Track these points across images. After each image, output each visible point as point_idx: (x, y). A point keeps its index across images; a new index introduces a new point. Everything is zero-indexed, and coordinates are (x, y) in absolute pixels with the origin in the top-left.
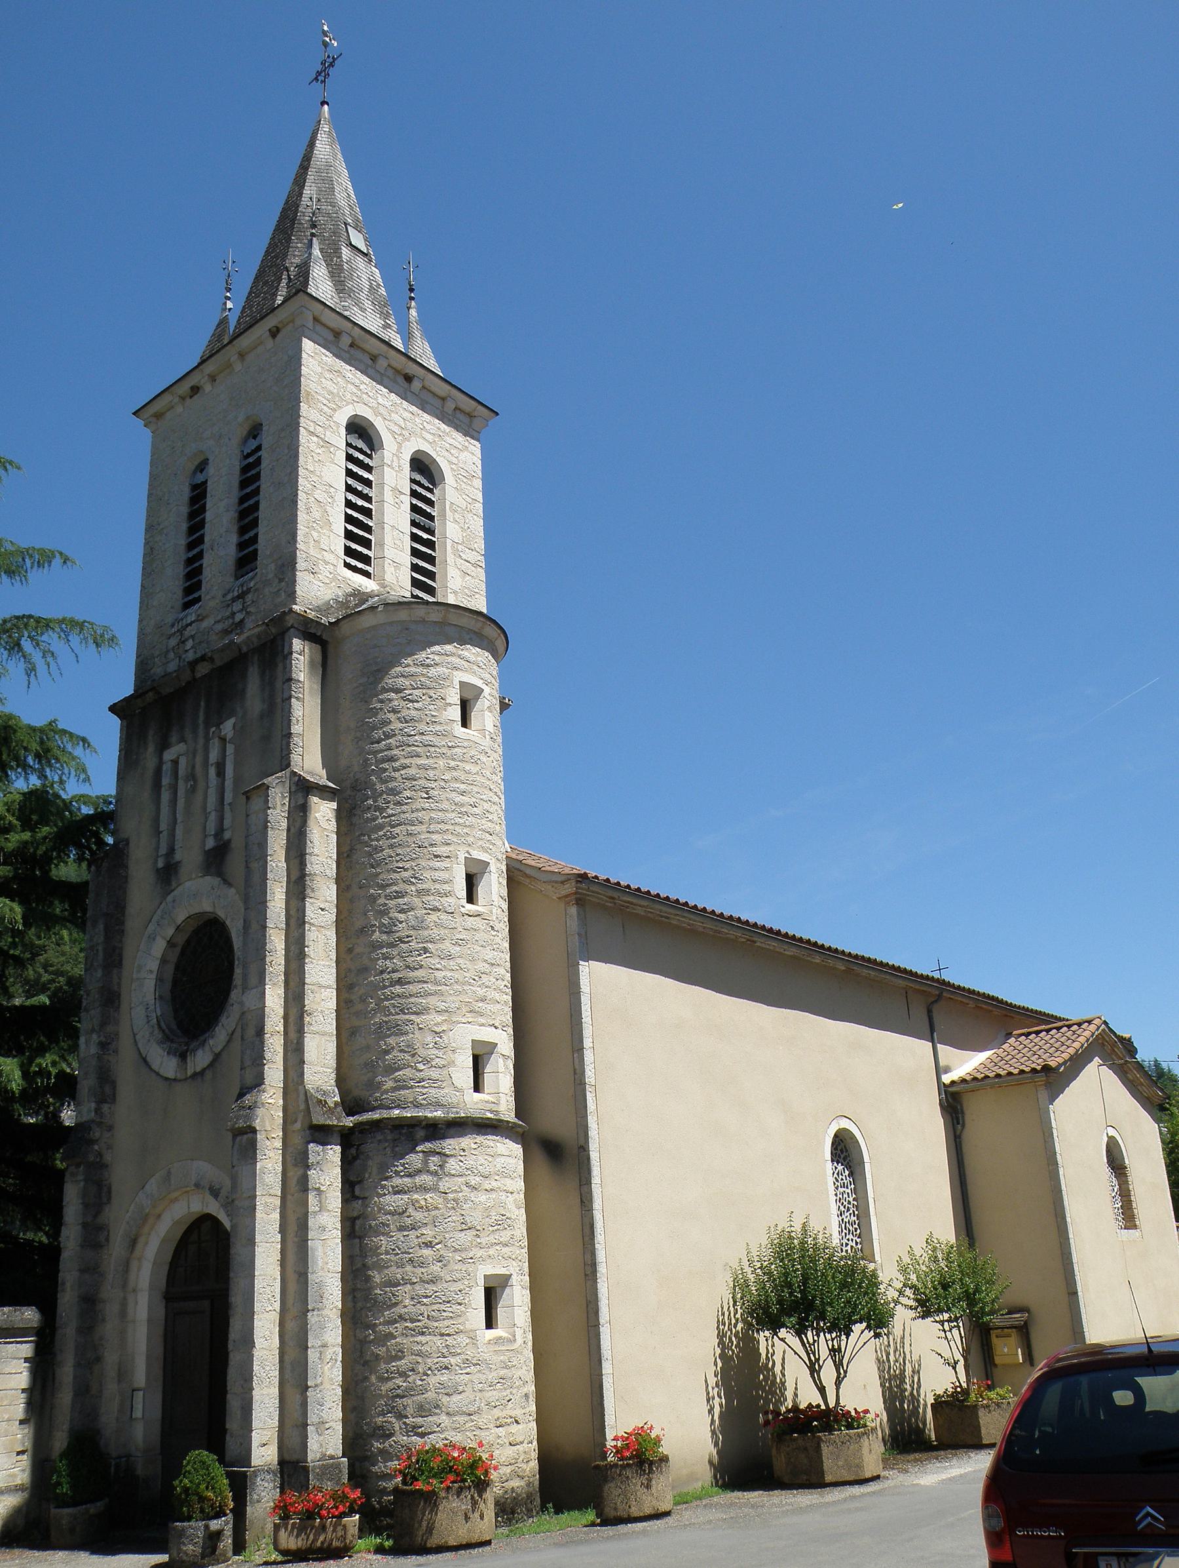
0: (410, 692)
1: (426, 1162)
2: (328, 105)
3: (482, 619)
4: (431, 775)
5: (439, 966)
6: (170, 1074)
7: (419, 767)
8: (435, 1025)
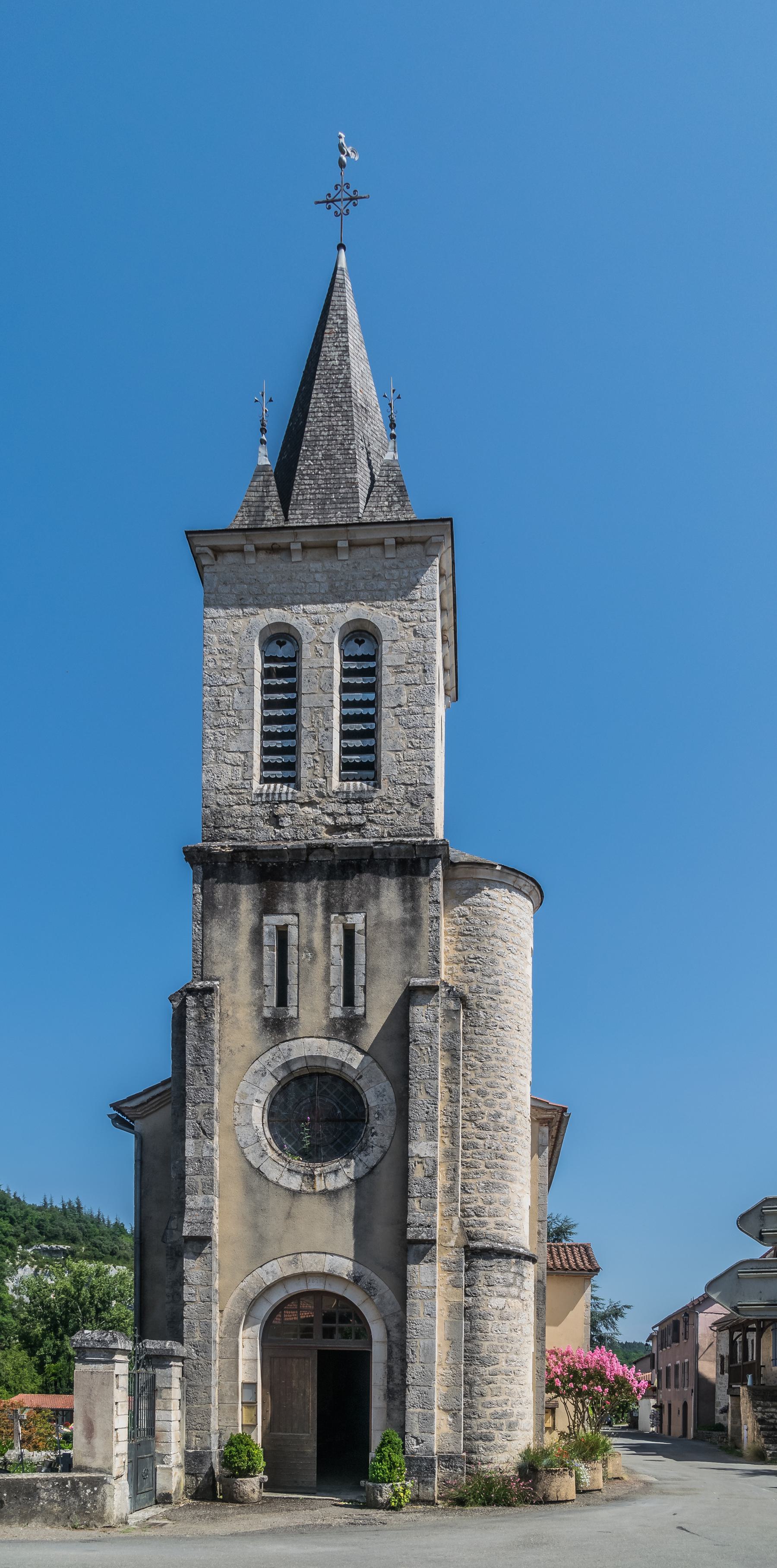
0: (511, 945)
7: (515, 1006)
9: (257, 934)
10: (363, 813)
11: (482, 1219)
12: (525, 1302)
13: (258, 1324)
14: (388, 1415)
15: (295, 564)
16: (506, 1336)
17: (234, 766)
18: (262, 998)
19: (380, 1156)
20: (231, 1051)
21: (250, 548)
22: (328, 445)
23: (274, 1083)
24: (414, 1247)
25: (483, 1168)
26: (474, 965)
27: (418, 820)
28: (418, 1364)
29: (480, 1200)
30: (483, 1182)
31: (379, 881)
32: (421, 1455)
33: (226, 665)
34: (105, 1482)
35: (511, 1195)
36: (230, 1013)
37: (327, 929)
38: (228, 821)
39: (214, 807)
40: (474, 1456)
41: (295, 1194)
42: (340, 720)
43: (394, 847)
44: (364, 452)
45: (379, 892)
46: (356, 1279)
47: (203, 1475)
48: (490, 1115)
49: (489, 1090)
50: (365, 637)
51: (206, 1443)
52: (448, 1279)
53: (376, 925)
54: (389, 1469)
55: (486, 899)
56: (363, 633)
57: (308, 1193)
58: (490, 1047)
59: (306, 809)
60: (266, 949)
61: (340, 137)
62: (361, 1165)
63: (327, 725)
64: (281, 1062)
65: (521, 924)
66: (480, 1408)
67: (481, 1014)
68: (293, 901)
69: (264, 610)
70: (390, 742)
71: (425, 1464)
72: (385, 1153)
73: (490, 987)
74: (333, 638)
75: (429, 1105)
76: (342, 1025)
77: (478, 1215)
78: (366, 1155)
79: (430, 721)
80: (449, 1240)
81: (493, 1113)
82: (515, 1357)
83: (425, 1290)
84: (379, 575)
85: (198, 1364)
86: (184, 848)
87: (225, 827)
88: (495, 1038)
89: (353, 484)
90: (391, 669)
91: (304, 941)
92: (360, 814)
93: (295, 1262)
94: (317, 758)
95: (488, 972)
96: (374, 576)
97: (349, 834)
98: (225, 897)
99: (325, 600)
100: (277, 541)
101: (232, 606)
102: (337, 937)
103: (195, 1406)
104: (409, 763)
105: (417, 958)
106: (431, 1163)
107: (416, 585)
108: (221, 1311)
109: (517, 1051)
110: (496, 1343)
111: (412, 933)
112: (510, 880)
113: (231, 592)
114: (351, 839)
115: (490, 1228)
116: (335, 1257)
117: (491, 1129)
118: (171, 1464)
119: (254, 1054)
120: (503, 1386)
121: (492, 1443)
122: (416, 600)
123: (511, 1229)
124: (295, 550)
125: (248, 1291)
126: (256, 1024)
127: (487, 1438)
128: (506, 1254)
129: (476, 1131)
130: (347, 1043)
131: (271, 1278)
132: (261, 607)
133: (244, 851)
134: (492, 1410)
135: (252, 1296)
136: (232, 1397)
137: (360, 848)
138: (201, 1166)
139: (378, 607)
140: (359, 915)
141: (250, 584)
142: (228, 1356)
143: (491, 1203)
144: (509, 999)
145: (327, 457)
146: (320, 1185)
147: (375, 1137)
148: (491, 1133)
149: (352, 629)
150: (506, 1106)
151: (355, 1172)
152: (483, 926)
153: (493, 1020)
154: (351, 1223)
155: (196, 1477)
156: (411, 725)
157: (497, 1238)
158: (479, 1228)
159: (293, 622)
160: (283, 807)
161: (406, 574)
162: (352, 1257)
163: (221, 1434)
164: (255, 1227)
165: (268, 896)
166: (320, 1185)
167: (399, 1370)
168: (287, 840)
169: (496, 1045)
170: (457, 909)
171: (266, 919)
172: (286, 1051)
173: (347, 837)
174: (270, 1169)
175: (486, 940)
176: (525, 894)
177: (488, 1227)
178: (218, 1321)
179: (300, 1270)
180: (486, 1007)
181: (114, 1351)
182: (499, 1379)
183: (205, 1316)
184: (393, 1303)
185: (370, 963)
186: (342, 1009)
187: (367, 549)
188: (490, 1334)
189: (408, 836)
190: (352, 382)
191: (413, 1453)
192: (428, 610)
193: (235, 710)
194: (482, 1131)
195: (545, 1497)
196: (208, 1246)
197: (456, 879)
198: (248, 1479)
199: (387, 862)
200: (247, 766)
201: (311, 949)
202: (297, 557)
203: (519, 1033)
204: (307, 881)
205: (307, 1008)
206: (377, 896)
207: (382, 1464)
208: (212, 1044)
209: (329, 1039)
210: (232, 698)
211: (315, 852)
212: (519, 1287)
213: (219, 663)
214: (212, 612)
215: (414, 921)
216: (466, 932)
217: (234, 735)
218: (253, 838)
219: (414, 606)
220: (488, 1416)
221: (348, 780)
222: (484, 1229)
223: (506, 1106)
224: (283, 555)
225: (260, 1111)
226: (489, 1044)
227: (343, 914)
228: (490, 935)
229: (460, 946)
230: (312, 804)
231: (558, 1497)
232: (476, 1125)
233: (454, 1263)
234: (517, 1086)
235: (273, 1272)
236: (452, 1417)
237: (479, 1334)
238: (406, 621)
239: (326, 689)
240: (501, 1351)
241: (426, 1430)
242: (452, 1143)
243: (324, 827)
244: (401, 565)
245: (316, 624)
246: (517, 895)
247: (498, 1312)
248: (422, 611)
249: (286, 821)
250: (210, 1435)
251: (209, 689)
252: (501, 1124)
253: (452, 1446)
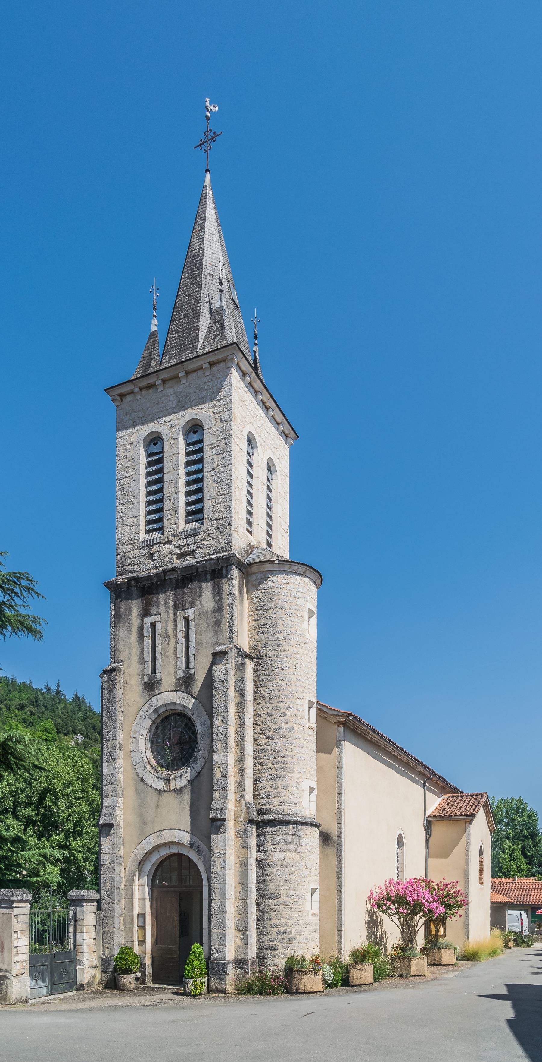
0: (289, 611)
1: (292, 839)
2: (210, 173)
3: (318, 575)
4: (297, 657)
5: (298, 752)
6: (160, 788)
7: (292, 652)
8: (296, 779)
9: (141, 628)
10: (195, 543)
11: (270, 800)
12: (302, 855)
15: (160, 393)
16: (286, 878)
17: (131, 526)
18: (143, 670)
19: (203, 764)
20: (129, 705)
21: (137, 390)
22: (187, 307)
23: (151, 722)
25: (270, 765)
26: (264, 629)
27: (223, 542)
28: (217, 900)
29: (268, 787)
30: (270, 775)
31: (202, 586)
32: (218, 960)
33: (127, 465)
34: (7, 978)
35: (290, 782)
36: (128, 682)
37: (175, 621)
38: (128, 561)
39: (122, 554)
40: (265, 961)
41: (160, 792)
42: (185, 485)
43: (207, 563)
44: (208, 305)
45: (201, 593)
46: (192, 845)
47: (110, 973)
48: (275, 729)
49: (273, 712)
50: (198, 429)
52: (240, 842)
53: (200, 614)
55: (271, 584)
56: (196, 426)
57: (167, 792)
58: (274, 683)
59: (167, 546)
60: (145, 638)
61: (206, 101)
62: (193, 771)
63: (176, 491)
64: (153, 709)
65: (297, 596)
66: (269, 928)
67: (269, 661)
68: (158, 606)
69: (145, 426)
70: (209, 493)
72: (206, 762)
73: (274, 642)
74: (179, 434)
75: (223, 729)
76: (183, 682)
77: (267, 797)
78: (196, 764)
79: (229, 475)
80: (240, 817)
81: (276, 727)
82: (293, 892)
83: (220, 851)
84: (202, 388)
85: (108, 903)
86: (104, 583)
87: (127, 565)
88: (278, 676)
89: (197, 330)
90: (209, 447)
91: (164, 631)
92: (194, 544)
93: (161, 836)
94: (172, 512)
95: (272, 632)
96: (200, 389)
97: (188, 558)
98: (125, 610)
99: (175, 412)
100: (149, 382)
101: (130, 427)
102: (181, 626)
104: (218, 505)
105: (221, 632)
106: (224, 767)
107: (221, 389)
108: (125, 869)
109: (294, 683)
110: (278, 883)
111: (218, 616)
112: (287, 567)
113: (129, 419)
114: (190, 561)
115: (276, 806)
117: (275, 738)
118: (84, 966)
119: (140, 706)
120: (284, 913)
121: (277, 952)
122: (221, 399)
123: (291, 804)
124: (159, 385)
126: (141, 687)
127: (273, 949)
128: (286, 823)
129: (266, 740)
130: (185, 692)
131: (149, 846)
132: (143, 424)
133: (133, 579)
134: (276, 930)
135: (140, 859)
137: (190, 566)
138: (110, 780)
139: (202, 409)
140: (191, 609)
141: (139, 411)
143: (275, 789)
144: (287, 648)
145: (186, 316)
146: (173, 786)
147: (200, 752)
148: (275, 741)
149: (190, 426)
150: (285, 721)
151: (191, 775)
152: (269, 602)
153: (276, 664)
154: (189, 809)
155: (107, 974)
156: (219, 480)
157: (280, 812)
158: (268, 806)
159: (159, 429)
160: (155, 547)
161: (216, 384)
162: (190, 832)
164: (141, 815)
165: (146, 606)
166: (173, 786)
168: (157, 567)
169: (278, 681)
170: (254, 593)
171: (145, 619)
172: (155, 702)
173: (187, 560)
174: (148, 777)
175: (271, 611)
176: (300, 574)
177: (274, 804)
179: (163, 841)
180: (271, 656)
181: (13, 901)
182: (281, 908)
185: (197, 640)
186: (183, 671)
187: (196, 373)
188: (275, 878)
189: (219, 553)
190: (204, 261)
191: (215, 959)
192: (228, 404)
193: (131, 492)
194: (269, 740)
195: (297, 990)
197: (253, 573)
198: (126, 975)
199: (206, 572)
200: (137, 525)
201: (168, 636)
202: (160, 389)
203: (296, 670)
204: (165, 592)
205: (166, 673)
206: (200, 596)
208: (115, 703)
209: (177, 691)
210: (129, 485)
211: (168, 574)
212: (296, 844)
213: (123, 464)
214: (120, 434)
215: (219, 609)
216: (259, 608)
217: (131, 507)
218: (140, 570)
219: (221, 403)
220: (274, 933)
221: (189, 522)
222: (271, 806)
223: (285, 721)
224: (154, 389)
225: (144, 741)
226: (274, 681)
227: (183, 610)
228: (274, 607)
229: (256, 618)
230: (169, 542)
231: (305, 990)
232: (266, 736)
234: (295, 706)
235: (150, 843)
236: (243, 935)
237: (268, 878)
238: (217, 414)
239: (176, 469)
240: (282, 889)
241: (222, 944)
242: (241, 752)
243: (175, 556)
244: (214, 378)
245: (170, 428)
246: (294, 576)
247: (280, 862)
248: (224, 405)
249: (156, 556)
251: (119, 481)
252: (282, 734)
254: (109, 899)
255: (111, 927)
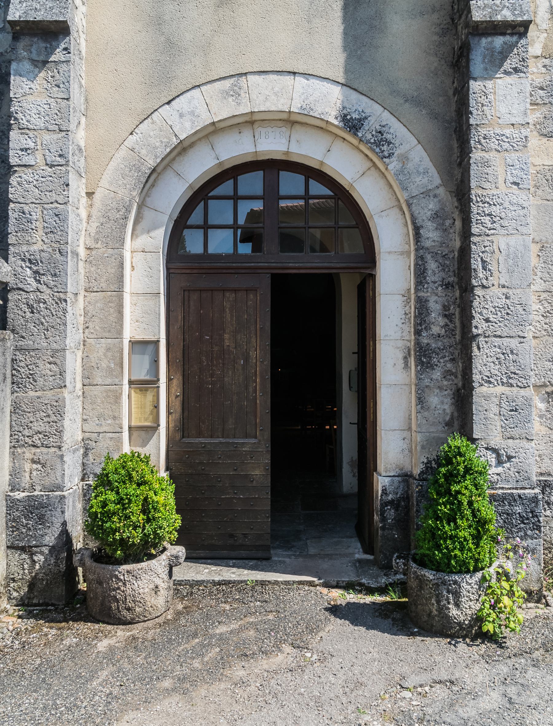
13: (163, 226)
14: (420, 400)
24: (484, 41)
47: (46, 550)
51: (52, 476)
54: (474, 537)
71: (519, 509)
83: (508, 132)
103: (32, 394)
108: (90, 194)
116: (313, 81)
125: (144, 152)
131: (188, 125)
135: (151, 162)
136: (110, 371)
142: (104, 285)
155: (32, 554)
163: (87, 450)
167: (439, 307)
178: (83, 214)
179: (244, 109)
183: (54, 197)
184: (426, 172)
196: (62, 46)
198: (143, 565)
207: (457, 527)
233: (542, 89)
235: (192, 113)
241: (516, 432)
250: (62, 457)
253: (546, 460)
254: (43, 288)
255: (49, 384)
